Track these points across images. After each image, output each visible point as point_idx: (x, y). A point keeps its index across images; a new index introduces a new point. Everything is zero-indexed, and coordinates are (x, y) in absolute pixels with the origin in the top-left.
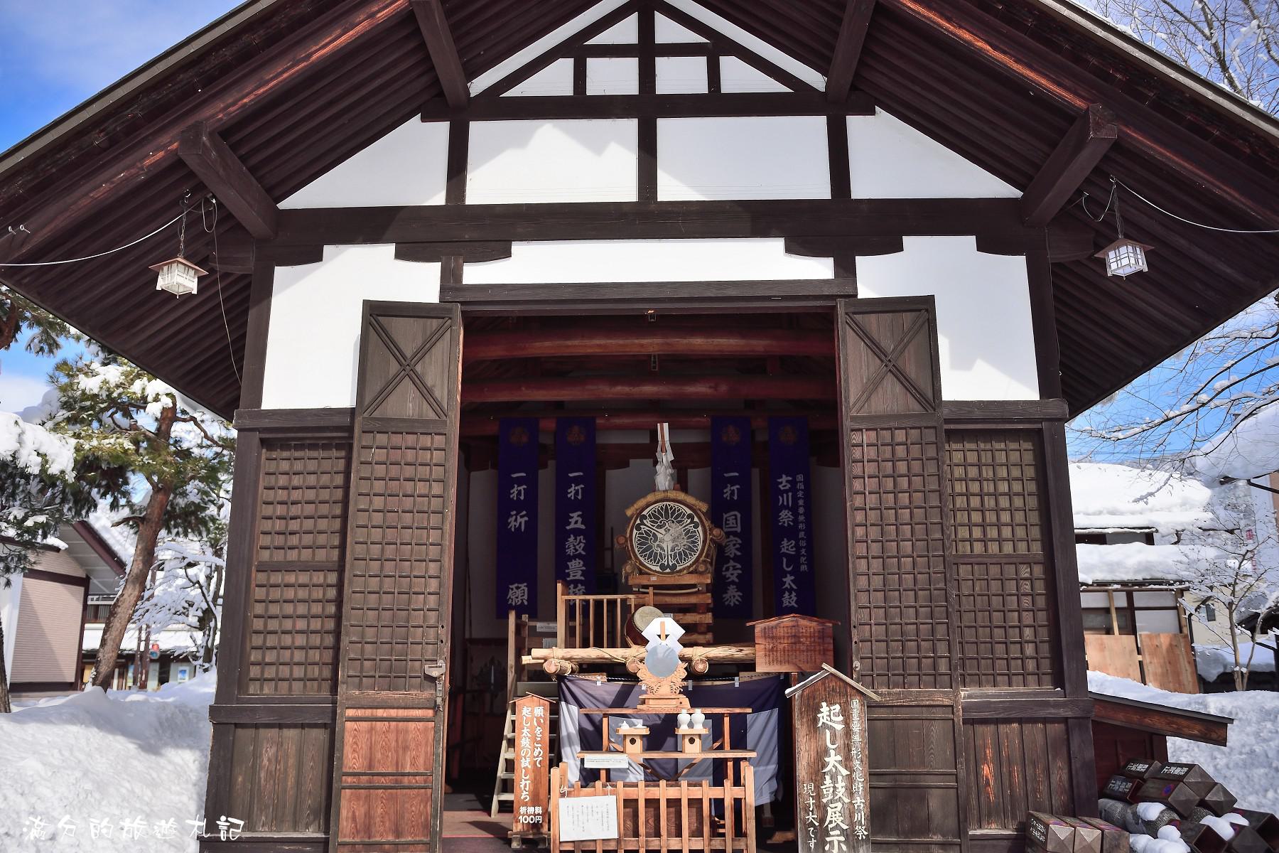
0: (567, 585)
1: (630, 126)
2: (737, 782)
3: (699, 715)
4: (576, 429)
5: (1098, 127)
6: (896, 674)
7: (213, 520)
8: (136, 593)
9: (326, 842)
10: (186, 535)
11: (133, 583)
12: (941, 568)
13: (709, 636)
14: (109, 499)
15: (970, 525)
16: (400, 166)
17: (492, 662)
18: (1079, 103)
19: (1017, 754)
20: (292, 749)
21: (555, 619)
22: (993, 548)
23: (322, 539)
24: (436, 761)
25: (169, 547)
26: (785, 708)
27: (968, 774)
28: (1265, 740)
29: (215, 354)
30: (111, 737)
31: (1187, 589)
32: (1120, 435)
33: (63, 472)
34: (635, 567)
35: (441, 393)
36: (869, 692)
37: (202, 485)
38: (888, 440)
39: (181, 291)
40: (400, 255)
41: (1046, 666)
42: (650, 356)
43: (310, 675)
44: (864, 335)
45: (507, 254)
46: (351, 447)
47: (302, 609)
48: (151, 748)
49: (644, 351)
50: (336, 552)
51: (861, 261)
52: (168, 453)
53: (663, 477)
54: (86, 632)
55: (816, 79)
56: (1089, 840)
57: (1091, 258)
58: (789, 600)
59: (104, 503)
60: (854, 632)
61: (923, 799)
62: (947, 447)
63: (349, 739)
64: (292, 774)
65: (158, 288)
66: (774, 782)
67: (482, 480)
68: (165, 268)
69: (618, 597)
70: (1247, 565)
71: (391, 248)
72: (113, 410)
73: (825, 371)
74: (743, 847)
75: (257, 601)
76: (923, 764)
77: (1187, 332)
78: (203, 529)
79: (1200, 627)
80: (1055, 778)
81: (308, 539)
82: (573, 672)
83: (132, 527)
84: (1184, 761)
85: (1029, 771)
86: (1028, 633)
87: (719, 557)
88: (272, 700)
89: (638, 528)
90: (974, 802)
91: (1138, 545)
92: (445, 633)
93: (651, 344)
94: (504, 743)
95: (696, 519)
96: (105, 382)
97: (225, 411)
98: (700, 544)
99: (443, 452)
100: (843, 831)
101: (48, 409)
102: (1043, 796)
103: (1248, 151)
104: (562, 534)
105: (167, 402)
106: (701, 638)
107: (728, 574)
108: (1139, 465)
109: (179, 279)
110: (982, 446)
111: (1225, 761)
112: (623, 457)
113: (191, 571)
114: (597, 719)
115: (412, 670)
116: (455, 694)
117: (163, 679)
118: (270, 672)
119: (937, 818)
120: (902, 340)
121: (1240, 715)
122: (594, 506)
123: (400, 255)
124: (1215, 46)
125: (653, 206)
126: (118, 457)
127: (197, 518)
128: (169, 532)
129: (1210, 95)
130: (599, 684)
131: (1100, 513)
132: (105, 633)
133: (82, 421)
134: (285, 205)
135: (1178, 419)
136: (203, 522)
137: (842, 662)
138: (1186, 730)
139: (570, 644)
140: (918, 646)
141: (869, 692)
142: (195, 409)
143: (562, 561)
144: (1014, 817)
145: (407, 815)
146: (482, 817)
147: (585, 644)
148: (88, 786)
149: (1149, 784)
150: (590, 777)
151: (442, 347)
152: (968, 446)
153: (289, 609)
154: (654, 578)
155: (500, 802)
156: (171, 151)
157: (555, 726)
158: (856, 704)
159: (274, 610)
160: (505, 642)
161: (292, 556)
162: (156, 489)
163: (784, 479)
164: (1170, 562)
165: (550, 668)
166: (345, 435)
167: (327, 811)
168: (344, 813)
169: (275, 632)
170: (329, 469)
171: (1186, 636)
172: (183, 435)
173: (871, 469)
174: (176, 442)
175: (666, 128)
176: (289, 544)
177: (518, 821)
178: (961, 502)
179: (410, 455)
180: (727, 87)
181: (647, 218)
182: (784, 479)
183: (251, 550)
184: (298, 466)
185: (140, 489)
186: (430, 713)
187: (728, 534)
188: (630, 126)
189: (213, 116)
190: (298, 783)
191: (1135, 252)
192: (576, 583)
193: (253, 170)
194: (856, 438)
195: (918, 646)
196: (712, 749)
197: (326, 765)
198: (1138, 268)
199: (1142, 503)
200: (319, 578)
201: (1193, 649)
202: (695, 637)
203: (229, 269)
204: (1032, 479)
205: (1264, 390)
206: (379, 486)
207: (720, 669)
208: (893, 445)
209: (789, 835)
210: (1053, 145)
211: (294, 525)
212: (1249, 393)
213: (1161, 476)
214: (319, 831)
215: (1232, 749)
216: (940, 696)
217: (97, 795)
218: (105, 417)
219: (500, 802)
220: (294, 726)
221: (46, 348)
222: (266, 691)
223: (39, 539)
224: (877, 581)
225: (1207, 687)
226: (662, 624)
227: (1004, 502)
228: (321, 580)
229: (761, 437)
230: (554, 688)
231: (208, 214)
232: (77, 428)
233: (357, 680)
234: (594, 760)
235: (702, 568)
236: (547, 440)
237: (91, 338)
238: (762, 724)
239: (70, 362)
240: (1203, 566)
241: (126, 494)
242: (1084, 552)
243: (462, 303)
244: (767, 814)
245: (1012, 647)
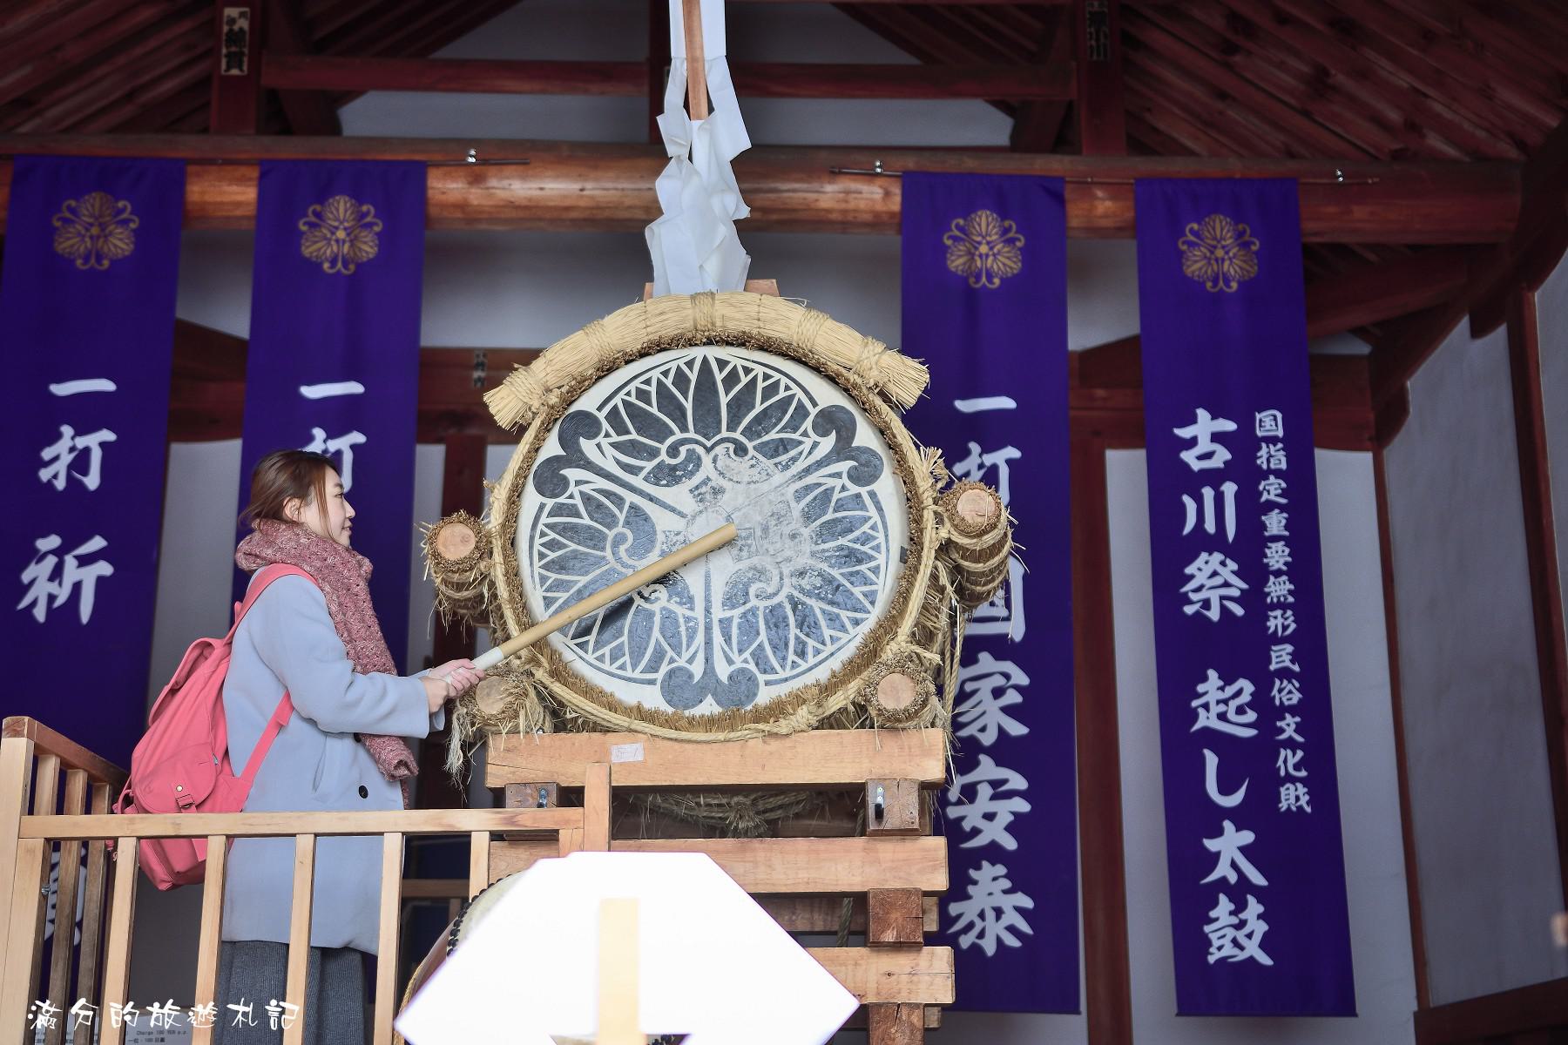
4: (341, 207)
89: (550, 479)
95: (865, 436)
98: (885, 586)
163: (1204, 426)
182: (1204, 426)
235: (896, 693)
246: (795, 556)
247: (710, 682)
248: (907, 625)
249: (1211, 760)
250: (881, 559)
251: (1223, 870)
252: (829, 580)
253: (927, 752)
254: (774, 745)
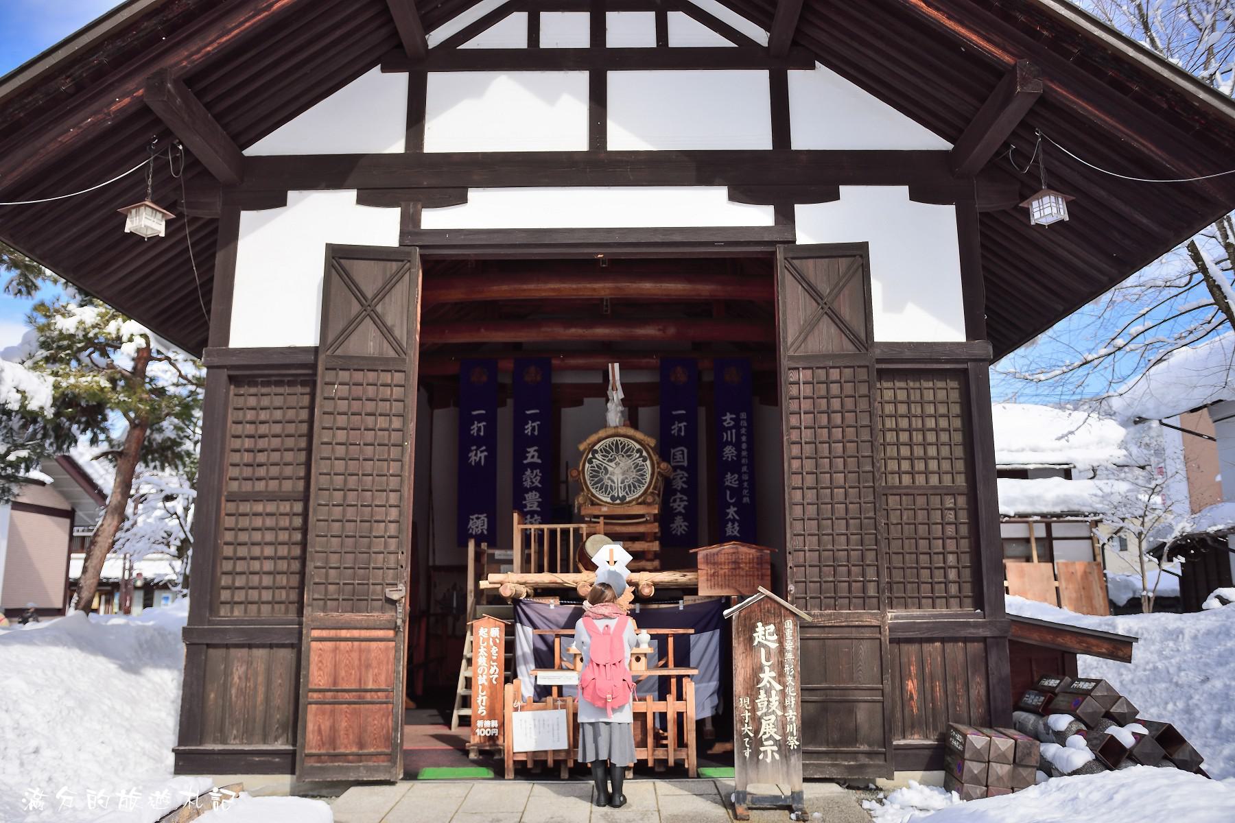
0: (523, 515)
1: (581, 78)
2: (680, 697)
3: (645, 635)
5: (1025, 81)
6: (827, 596)
7: (189, 454)
8: (115, 523)
9: (294, 753)
10: (163, 469)
11: (112, 514)
12: (871, 498)
13: (656, 563)
14: (89, 434)
15: (899, 459)
16: (362, 115)
17: (454, 588)
18: (1007, 58)
19: (939, 671)
20: (261, 668)
21: (511, 547)
22: (920, 480)
23: (288, 471)
24: (397, 678)
25: (154, 480)
26: (725, 627)
27: (893, 688)
28: (1166, 658)
29: (185, 295)
30: (92, 658)
31: (1101, 521)
32: (1042, 377)
33: (42, 408)
34: (586, 498)
35: (400, 332)
36: (802, 614)
37: (176, 421)
38: (823, 378)
39: (150, 234)
40: (361, 201)
41: (967, 589)
42: (602, 300)
43: (277, 599)
44: (802, 279)
45: (464, 200)
46: (315, 383)
47: (269, 537)
48: (131, 667)
49: (596, 295)
50: (301, 484)
51: (800, 209)
52: (143, 391)
53: (614, 414)
54: (72, 562)
55: (759, 35)
56: (1003, 748)
57: (1016, 208)
58: (732, 529)
59: (84, 439)
60: (789, 557)
61: (851, 712)
62: (878, 385)
63: (314, 658)
64: (261, 690)
65: (127, 230)
66: (715, 697)
67: (444, 419)
68: (134, 211)
69: (571, 526)
70: (1157, 499)
71: (353, 194)
72: (91, 350)
73: (764, 314)
74: (684, 757)
75: (227, 529)
76: (852, 680)
77: (1105, 279)
78: (179, 463)
79: (1112, 554)
80: (974, 693)
81: (274, 471)
82: (528, 596)
83: (111, 461)
84: (1093, 677)
85: (950, 686)
86: (951, 559)
87: (666, 490)
88: (242, 622)
89: (590, 462)
90: (898, 715)
91: (1058, 480)
92: (405, 558)
93: (602, 289)
94: (464, 662)
95: (645, 454)
96: (81, 322)
97: (195, 349)
98: (648, 480)
99: (402, 390)
100: (776, 741)
101: (27, 349)
102: (962, 709)
103: (1165, 106)
104: (519, 468)
105: (141, 342)
106: (649, 565)
107: (675, 505)
108: (1061, 406)
109: (147, 222)
110: (911, 384)
111: (1130, 677)
112: (577, 396)
113: (169, 504)
114: (550, 639)
115: (374, 592)
116: (415, 618)
117: (148, 603)
118: (240, 596)
119: (864, 728)
120: (837, 284)
121: (1146, 635)
122: (550, 442)
123: (361, 201)
124: (1139, 7)
125: (602, 156)
126: (94, 395)
127: (173, 452)
128: (147, 466)
129: (1131, 52)
130: (552, 607)
131: (1023, 450)
132: (86, 560)
133: (61, 360)
134: (250, 152)
135: (1096, 362)
136: (179, 456)
137: (778, 587)
138: (1095, 649)
139: (525, 569)
140: (849, 571)
141: (802, 614)
142: (168, 349)
143: (519, 492)
144: (935, 729)
145: (369, 729)
146: (443, 730)
147: (540, 570)
148: (71, 703)
149: (1060, 698)
150: (543, 692)
151: (400, 290)
152: (898, 384)
153: (257, 536)
154: (605, 509)
155: (460, 717)
156: (138, 97)
157: (510, 646)
158: (789, 624)
159: (243, 537)
160: (465, 568)
161: (260, 486)
162: (133, 425)
164: (1086, 495)
165: (506, 592)
166: (309, 372)
167: (294, 725)
168: (311, 726)
169: (244, 559)
170: (294, 404)
171: (1099, 564)
172: (160, 374)
173: (806, 405)
174: (152, 380)
175: (616, 80)
176: (257, 475)
177: (475, 734)
178: (891, 437)
179: (371, 391)
180: (675, 41)
181: (597, 166)
182: (728, 417)
183: (220, 481)
184: (265, 402)
185: (118, 425)
186: (391, 633)
187: (675, 468)
188: (581, 78)
189: (176, 64)
190: (267, 699)
191: (1057, 203)
192: (532, 513)
193: (218, 117)
194: (793, 376)
195: (849, 571)
196: (657, 667)
197: (293, 682)
198: (1059, 218)
199: (1063, 441)
200: (285, 507)
201: (1105, 575)
202: (643, 563)
203: (198, 213)
204: (957, 416)
205: (1176, 336)
206: (342, 420)
207: (665, 593)
208: (827, 383)
209: (728, 746)
210: (983, 100)
211: (262, 458)
212: (1161, 338)
213: (1080, 415)
214: (287, 743)
215: (1137, 666)
216: (868, 617)
217: (79, 712)
218: (84, 356)
219: (460, 717)
220: (263, 646)
221: (24, 289)
222: (236, 613)
223: (22, 473)
224: (812, 511)
225: (1117, 610)
226: (611, 551)
227: (931, 437)
228: (288, 509)
229: (708, 377)
230: (509, 611)
231: (175, 160)
232: (57, 367)
233: (321, 603)
234: (547, 678)
235: (650, 499)
236: (506, 379)
237: (68, 281)
238: (704, 644)
239: (47, 303)
240: (1116, 499)
241: (104, 430)
242: (1005, 487)
243: (421, 247)
244: (709, 726)
245: (936, 572)
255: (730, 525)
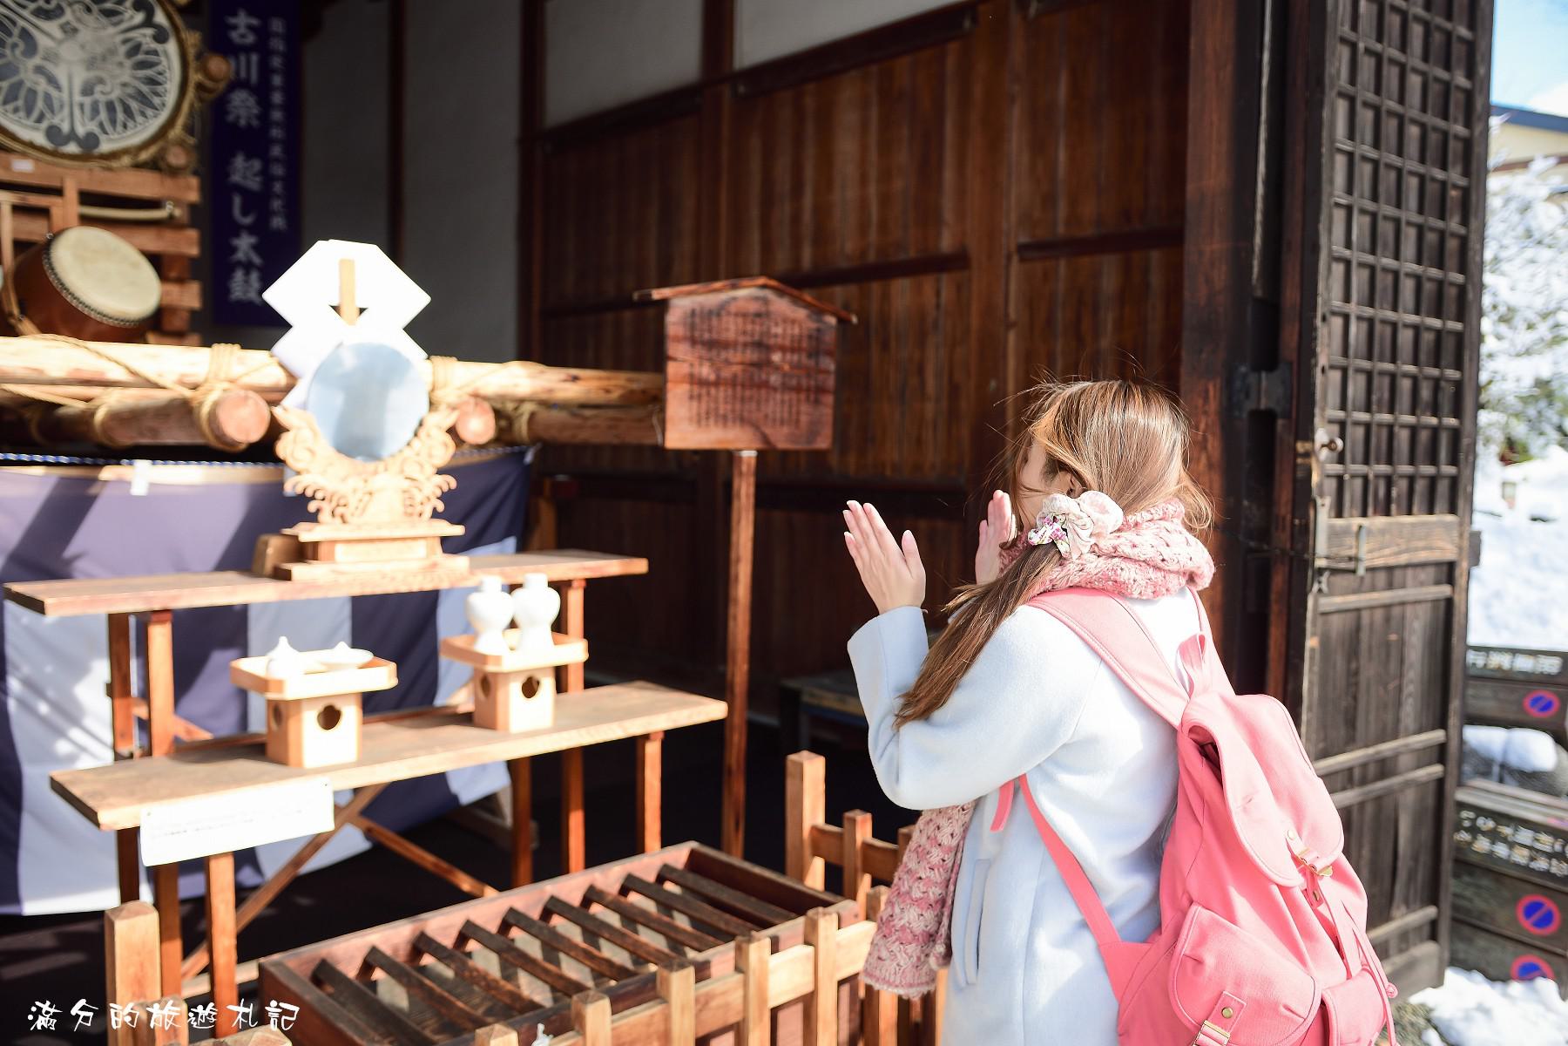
98: (171, 98)
197: (21, 373)
226: (346, 265)
235: (177, 158)
246: (120, 78)
247: (72, 136)
248: (180, 121)
249: (237, 201)
250: (168, 86)
251: (240, 256)
252: (140, 93)
253: (189, 188)
254: (108, 175)
255: (239, 275)
